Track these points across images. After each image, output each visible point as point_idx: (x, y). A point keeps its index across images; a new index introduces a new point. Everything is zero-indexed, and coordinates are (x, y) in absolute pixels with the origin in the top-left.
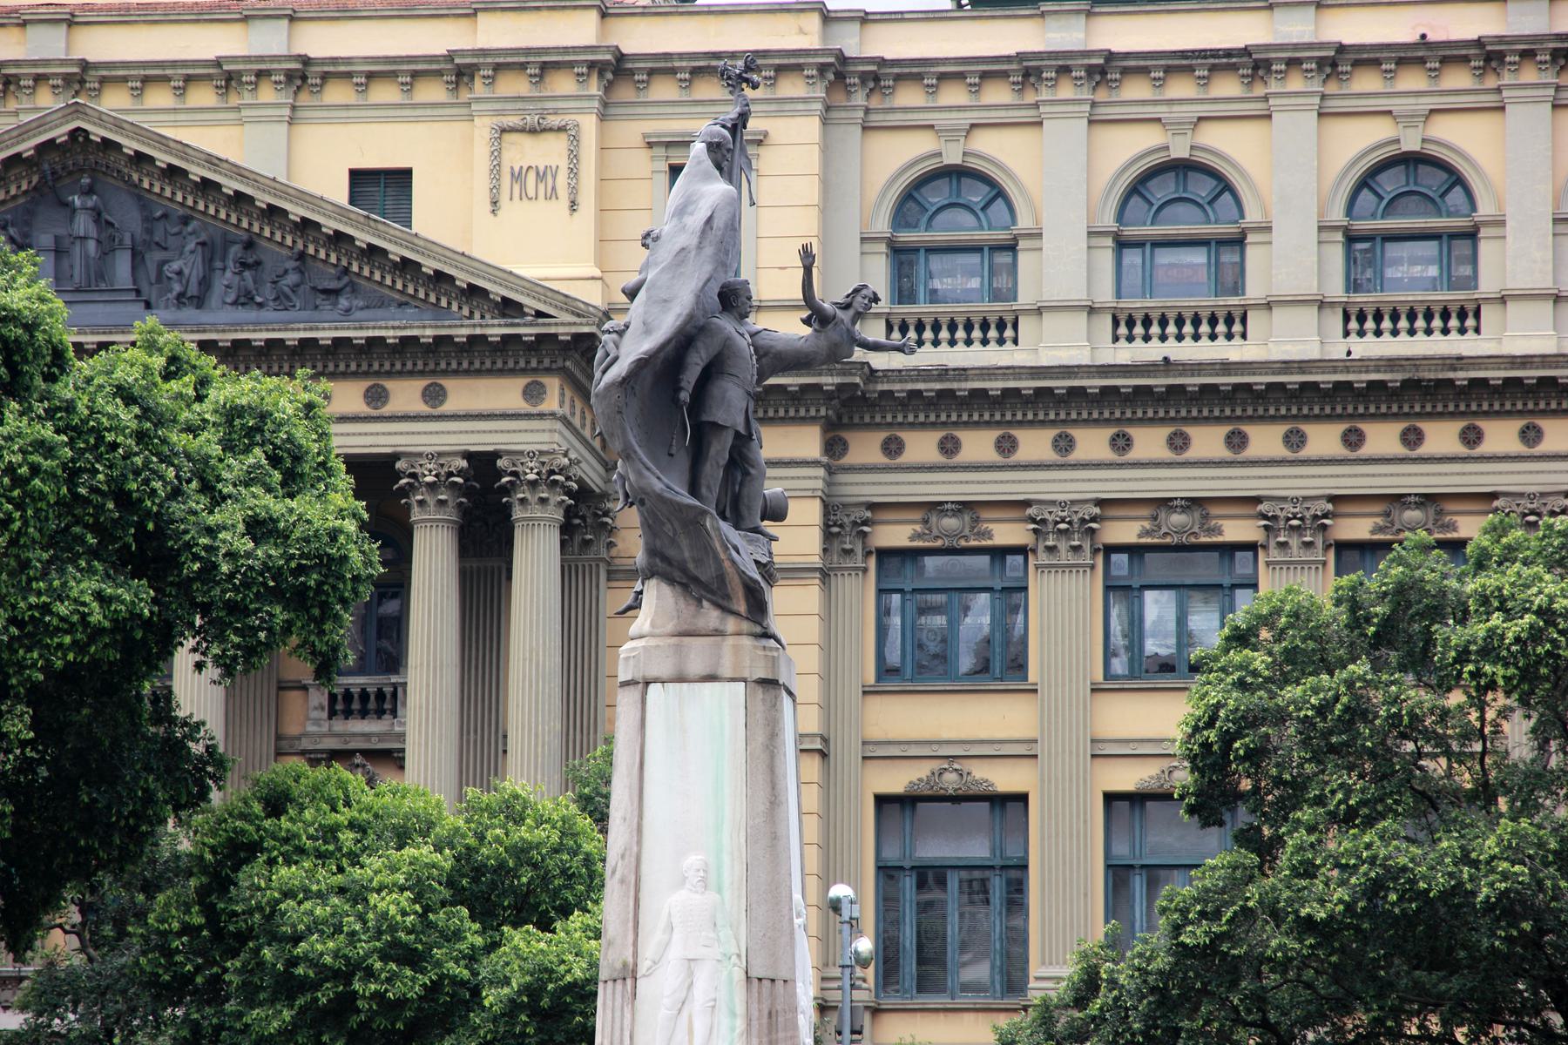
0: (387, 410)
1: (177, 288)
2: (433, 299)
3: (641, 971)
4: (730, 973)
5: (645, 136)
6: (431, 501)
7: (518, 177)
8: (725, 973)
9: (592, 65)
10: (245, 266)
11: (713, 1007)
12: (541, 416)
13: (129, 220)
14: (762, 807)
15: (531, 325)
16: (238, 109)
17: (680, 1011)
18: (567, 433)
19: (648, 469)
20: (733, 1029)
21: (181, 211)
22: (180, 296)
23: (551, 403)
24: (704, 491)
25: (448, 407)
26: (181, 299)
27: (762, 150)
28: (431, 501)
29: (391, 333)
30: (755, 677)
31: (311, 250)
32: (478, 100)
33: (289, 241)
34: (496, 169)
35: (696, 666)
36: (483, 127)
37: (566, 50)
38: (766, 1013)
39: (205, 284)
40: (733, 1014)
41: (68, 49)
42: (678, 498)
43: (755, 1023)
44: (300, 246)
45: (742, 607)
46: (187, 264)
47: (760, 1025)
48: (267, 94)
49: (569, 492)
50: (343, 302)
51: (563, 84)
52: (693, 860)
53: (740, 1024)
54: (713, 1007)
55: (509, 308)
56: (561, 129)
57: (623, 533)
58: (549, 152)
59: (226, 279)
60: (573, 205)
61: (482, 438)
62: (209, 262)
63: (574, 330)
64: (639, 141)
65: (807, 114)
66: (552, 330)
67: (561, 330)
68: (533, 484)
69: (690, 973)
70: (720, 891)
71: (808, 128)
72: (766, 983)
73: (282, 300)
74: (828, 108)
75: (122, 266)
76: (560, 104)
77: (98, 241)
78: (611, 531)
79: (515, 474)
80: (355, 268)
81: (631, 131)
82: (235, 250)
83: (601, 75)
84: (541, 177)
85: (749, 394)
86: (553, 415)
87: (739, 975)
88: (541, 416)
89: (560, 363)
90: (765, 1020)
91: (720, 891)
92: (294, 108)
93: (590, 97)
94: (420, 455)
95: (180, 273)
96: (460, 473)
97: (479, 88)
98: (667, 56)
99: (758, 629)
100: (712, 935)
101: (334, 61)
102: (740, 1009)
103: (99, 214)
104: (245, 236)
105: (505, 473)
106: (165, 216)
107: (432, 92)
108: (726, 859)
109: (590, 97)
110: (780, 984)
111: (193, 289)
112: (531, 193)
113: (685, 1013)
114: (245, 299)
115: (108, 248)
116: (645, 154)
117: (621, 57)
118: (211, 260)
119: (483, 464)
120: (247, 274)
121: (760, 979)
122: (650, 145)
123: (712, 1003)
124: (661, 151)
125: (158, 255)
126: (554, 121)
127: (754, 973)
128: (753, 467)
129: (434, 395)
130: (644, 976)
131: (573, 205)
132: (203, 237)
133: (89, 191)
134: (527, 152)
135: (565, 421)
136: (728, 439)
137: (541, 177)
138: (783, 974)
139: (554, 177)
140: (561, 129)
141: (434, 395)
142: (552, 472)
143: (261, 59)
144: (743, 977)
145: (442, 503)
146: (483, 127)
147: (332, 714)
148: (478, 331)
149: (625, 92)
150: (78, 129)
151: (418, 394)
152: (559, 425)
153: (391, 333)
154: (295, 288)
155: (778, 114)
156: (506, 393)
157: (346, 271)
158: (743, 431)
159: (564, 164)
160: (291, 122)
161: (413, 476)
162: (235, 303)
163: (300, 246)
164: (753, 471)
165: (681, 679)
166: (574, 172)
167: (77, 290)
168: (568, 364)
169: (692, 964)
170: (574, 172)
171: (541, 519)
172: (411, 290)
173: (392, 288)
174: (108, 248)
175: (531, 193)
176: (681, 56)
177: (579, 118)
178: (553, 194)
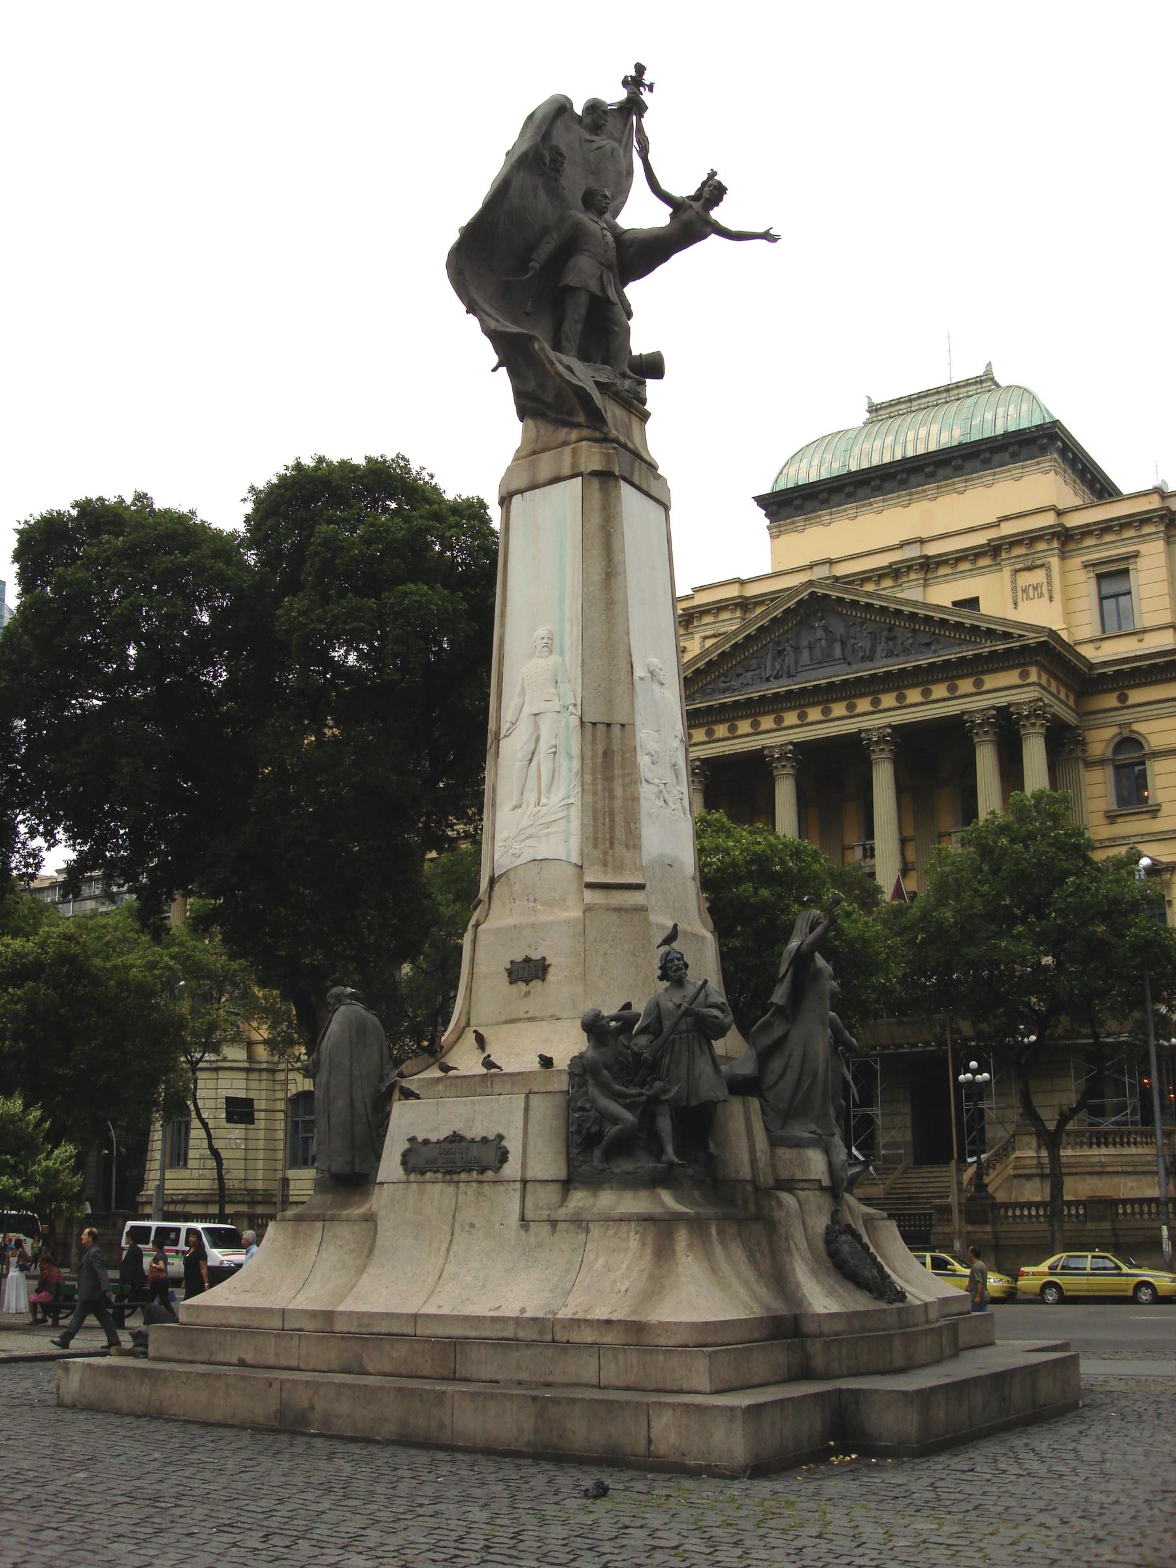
0: (958, 693)
1: (861, 654)
2: (973, 639)
3: (503, 732)
4: (567, 722)
5: (1083, 562)
6: (981, 732)
7: (1025, 591)
8: (563, 722)
9: (1053, 535)
10: (889, 639)
11: (555, 753)
12: (1028, 685)
13: (839, 628)
14: (597, 577)
15: (1017, 641)
16: (901, 585)
17: (531, 760)
18: (1041, 690)
19: (489, 315)
20: (570, 770)
21: (860, 620)
22: (862, 658)
23: (1033, 678)
24: (564, 343)
25: (986, 688)
26: (863, 659)
27: (1138, 560)
28: (981, 732)
29: (953, 656)
30: (589, 470)
31: (917, 627)
32: (1003, 560)
33: (907, 625)
34: (1014, 589)
35: (544, 474)
36: (1007, 572)
37: (1040, 529)
38: (600, 752)
39: (873, 650)
40: (570, 757)
41: (830, 573)
42: (508, 330)
43: (588, 762)
44: (912, 626)
45: (581, 418)
46: (865, 643)
47: (594, 764)
48: (913, 576)
49: (1048, 721)
50: (933, 648)
51: (1041, 546)
52: (541, 632)
53: (576, 764)
54: (555, 753)
55: (1007, 636)
56: (1042, 566)
57: (1090, 745)
58: (1038, 576)
59: (880, 648)
60: (1051, 599)
61: (1001, 700)
62: (874, 640)
63: (1037, 640)
64: (1079, 565)
65: (1157, 539)
66: (1027, 642)
67: (1031, 641)
68: (1027, 717)
69: (537, 727)
70: (562, 654)
71: (1159, 545)
72: (601, 728)
73: (907, 651)
74: (1169, 537)
75: (837, 651)
76: (1042, 554)
77: (826, 640)
78: (1085, 744)
79: (1018, 714)
80: (937, 632)
81: (1076, 562)
82: (885, 633)
83: (1058, 539)
84: (1035, 589)
85: (602, 264)
86: (1033, 684)
87: (574, 721)
88: (1028, 685)
89: (1034, 659)
90: (600, 759)
91: (562, 654)
92: (925, 580)
93: (1054, 549)
94: (973, 711)
95: (861, 647)
96: (993, 716)
97: (1004, 555)
98: (1088, 525)
99: (597, 435)
100: (553, 690)
101: (939, 555)
102: (575, 750)
103: (826, 628)
104: (888, 626)
105: (1013, 714)
106: (854, 624)
107: (984, 562)
108: (567, 626)
109: (1054, 549)
110: (616, 730)
111: (868, 653)
112: (1032, 597)
113: (534, 762)
114: (890, 654)
115: (830, 643)
116: (1084, 571)
117: (1067, 529)
118: (875, 639)
119: (1003, 712)
120: (890, 642)
121: (594, 724)
122: (1086, 567)
123: (554, 750)
124: (1091, 569)
125: (852, 641)
126: (1039, 562)
127: (586, 719)
128: (617, 325)
129: (979, 683)
130: (505, 736)
131: (1051, 599)
132: (870, 630)
133: (822, 619)
134: (1025, 579)
135: (1039, 685)
136: (583, 300)
137: (1035, 589)
138: (620, 717)
139: (1041, 587)
140: (1042, 566)
141: (979, 683)
142: (1035, 710)
143: (907, 560)
144: (578, 723)
145: (986, 732)
146: (1007, 572)
147: (963, 845)
148: (993, 649)
149: (1072, 546)
150: (813, 592)
151: (971, 684)
152: (1037, 688)
153: (953, 656)
154: (911, 645)
155: (1144, 542)
156: (1011, 677)
157: (934, 633)
158: (599, 293)
159: (1045, 581)
160: (925, 586)
161: (972, 722)
162: (886, 657)
163: (912, 626)
164: (616, 329)
165: (534, 487)
166: (1049, 583)
167: (819, 663)
168: (1039, 658)
169: (538, 718)
170: (1049, 583)
171: (1032, 733)
172: (963, 637)
173: (954, 637)
174: (830, 643)
175: (1032, 597)
176: (1095, 524)
177: (1050, 559)
178: (1041, 595)
